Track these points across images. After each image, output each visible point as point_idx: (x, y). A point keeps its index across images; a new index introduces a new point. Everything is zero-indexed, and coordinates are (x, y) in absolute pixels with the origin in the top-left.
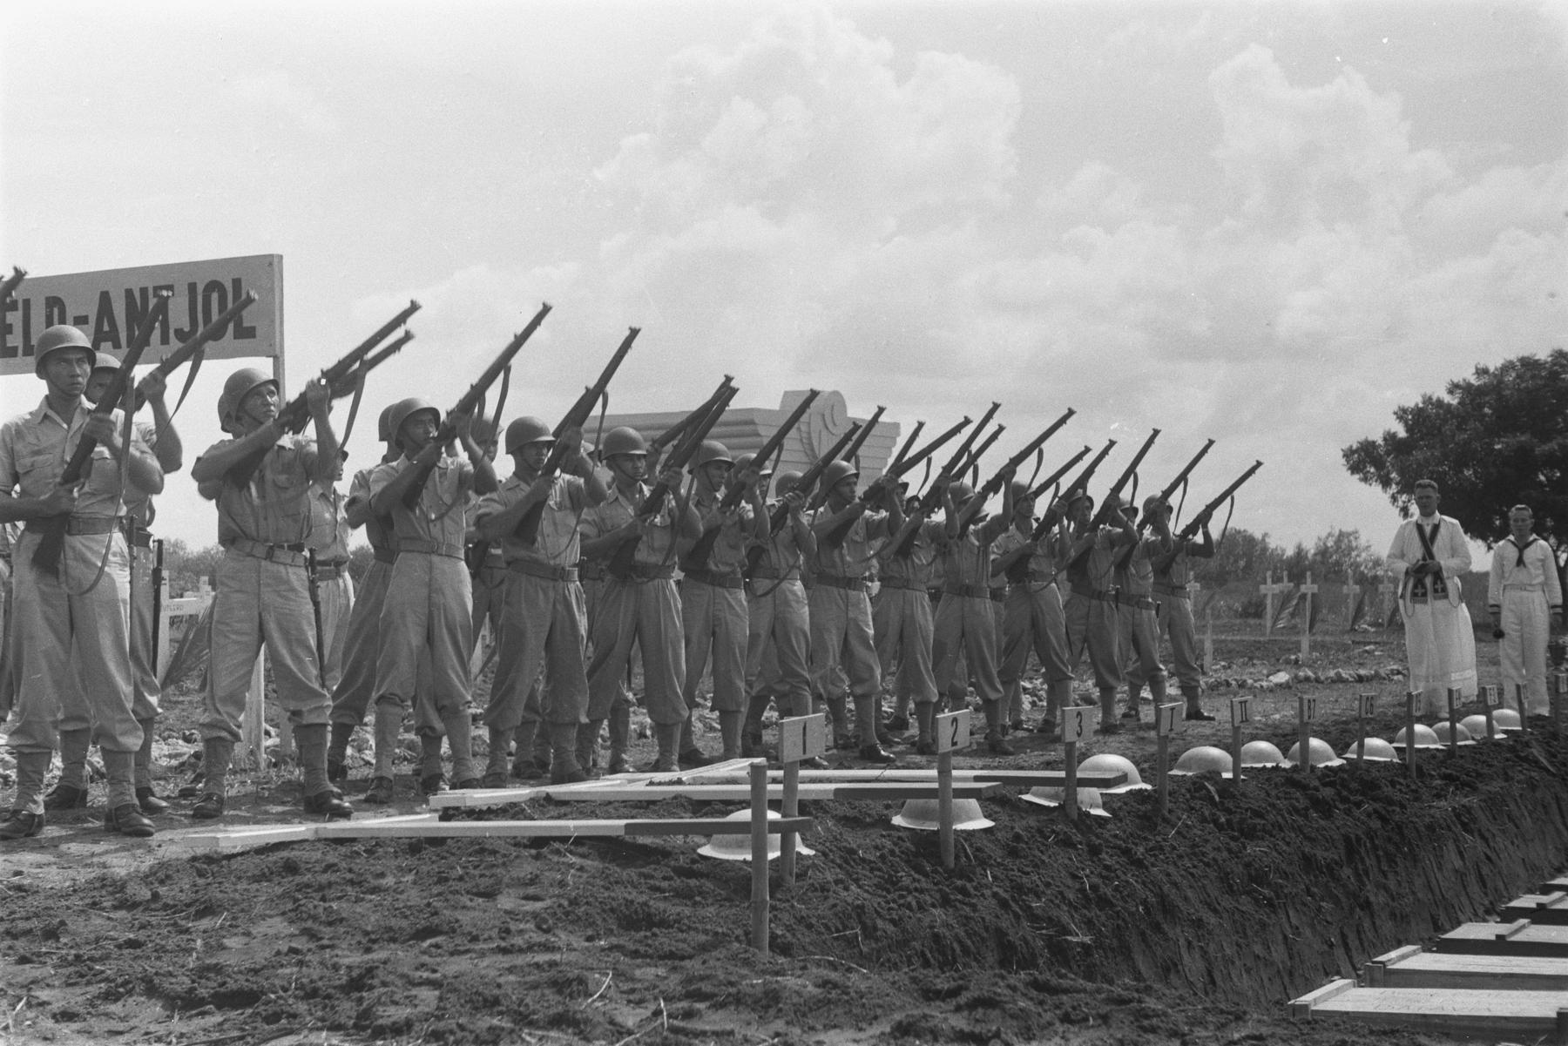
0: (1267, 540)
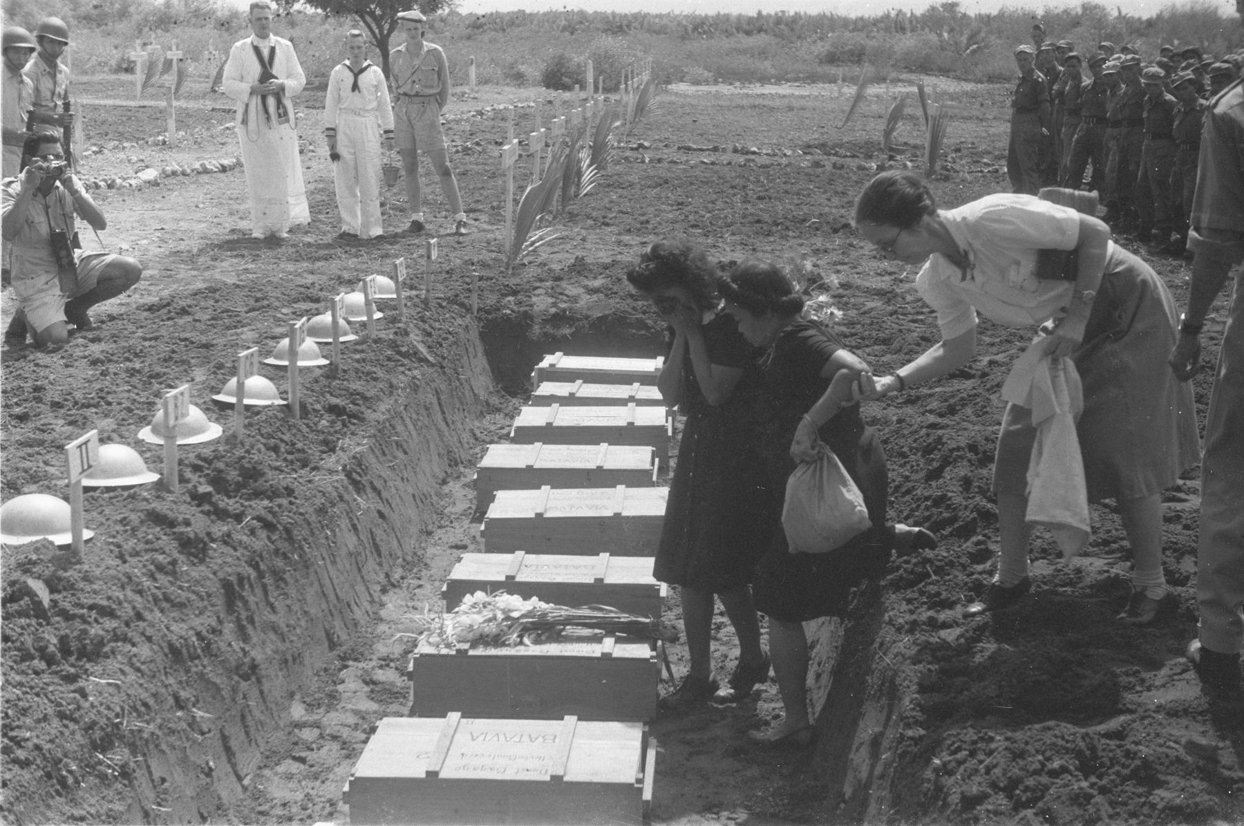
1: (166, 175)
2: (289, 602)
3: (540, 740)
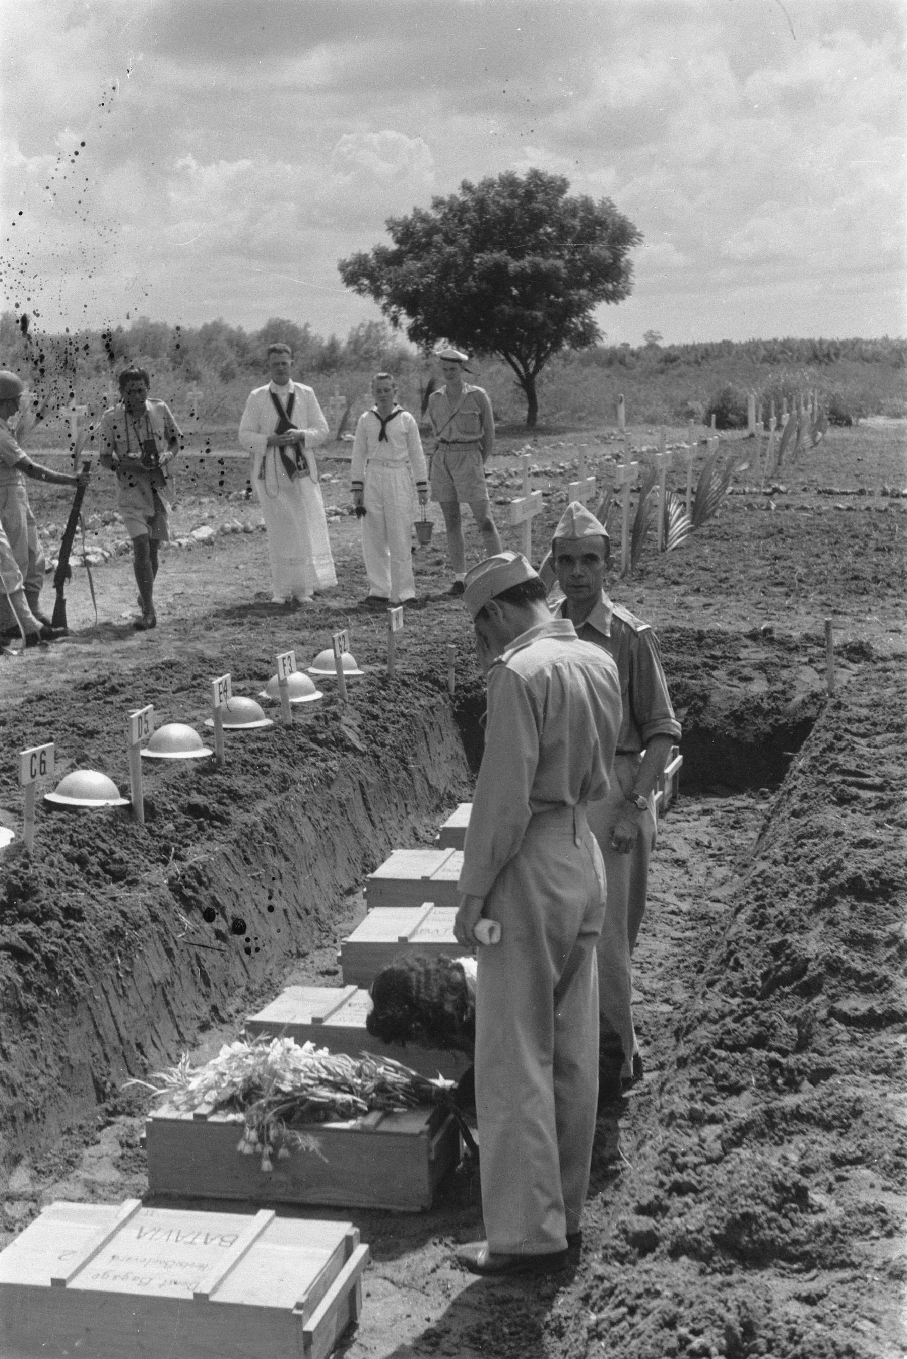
0: (309, 329)
1: (224, 533)
2: (35, 1047)
3: (217, 1241)
